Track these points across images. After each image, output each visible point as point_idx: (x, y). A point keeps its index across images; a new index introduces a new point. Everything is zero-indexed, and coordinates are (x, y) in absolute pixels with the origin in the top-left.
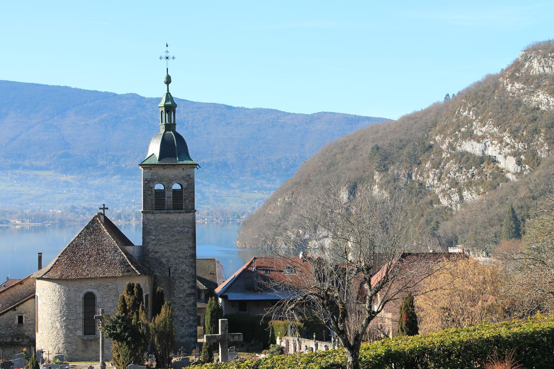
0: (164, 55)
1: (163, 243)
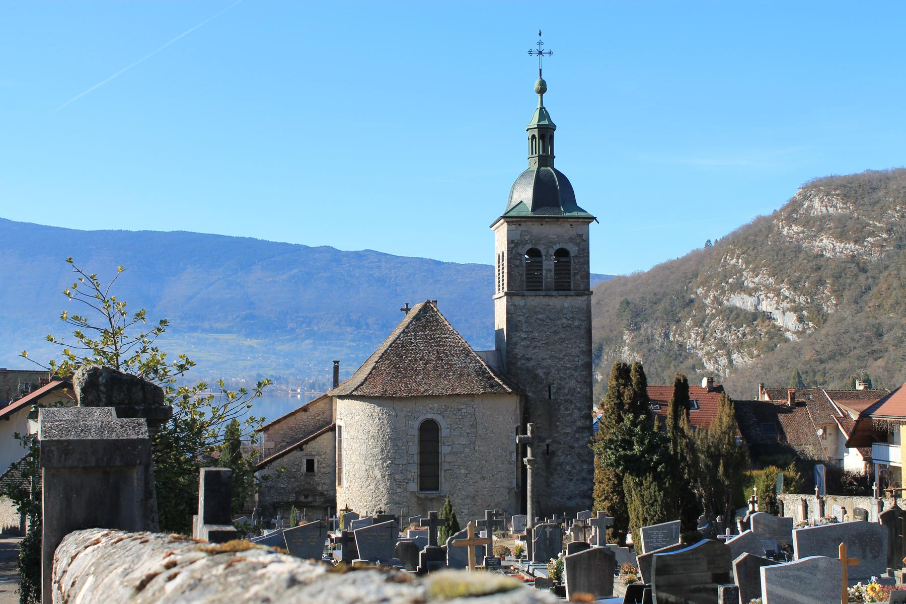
0: (535, 48)
1: (539, 344)
